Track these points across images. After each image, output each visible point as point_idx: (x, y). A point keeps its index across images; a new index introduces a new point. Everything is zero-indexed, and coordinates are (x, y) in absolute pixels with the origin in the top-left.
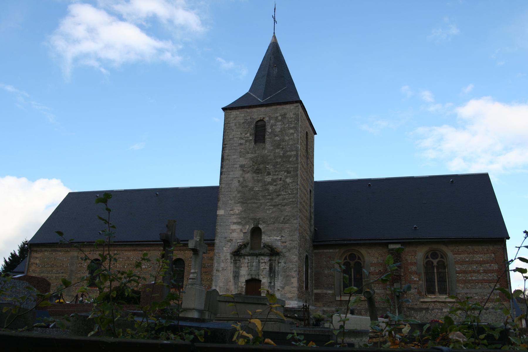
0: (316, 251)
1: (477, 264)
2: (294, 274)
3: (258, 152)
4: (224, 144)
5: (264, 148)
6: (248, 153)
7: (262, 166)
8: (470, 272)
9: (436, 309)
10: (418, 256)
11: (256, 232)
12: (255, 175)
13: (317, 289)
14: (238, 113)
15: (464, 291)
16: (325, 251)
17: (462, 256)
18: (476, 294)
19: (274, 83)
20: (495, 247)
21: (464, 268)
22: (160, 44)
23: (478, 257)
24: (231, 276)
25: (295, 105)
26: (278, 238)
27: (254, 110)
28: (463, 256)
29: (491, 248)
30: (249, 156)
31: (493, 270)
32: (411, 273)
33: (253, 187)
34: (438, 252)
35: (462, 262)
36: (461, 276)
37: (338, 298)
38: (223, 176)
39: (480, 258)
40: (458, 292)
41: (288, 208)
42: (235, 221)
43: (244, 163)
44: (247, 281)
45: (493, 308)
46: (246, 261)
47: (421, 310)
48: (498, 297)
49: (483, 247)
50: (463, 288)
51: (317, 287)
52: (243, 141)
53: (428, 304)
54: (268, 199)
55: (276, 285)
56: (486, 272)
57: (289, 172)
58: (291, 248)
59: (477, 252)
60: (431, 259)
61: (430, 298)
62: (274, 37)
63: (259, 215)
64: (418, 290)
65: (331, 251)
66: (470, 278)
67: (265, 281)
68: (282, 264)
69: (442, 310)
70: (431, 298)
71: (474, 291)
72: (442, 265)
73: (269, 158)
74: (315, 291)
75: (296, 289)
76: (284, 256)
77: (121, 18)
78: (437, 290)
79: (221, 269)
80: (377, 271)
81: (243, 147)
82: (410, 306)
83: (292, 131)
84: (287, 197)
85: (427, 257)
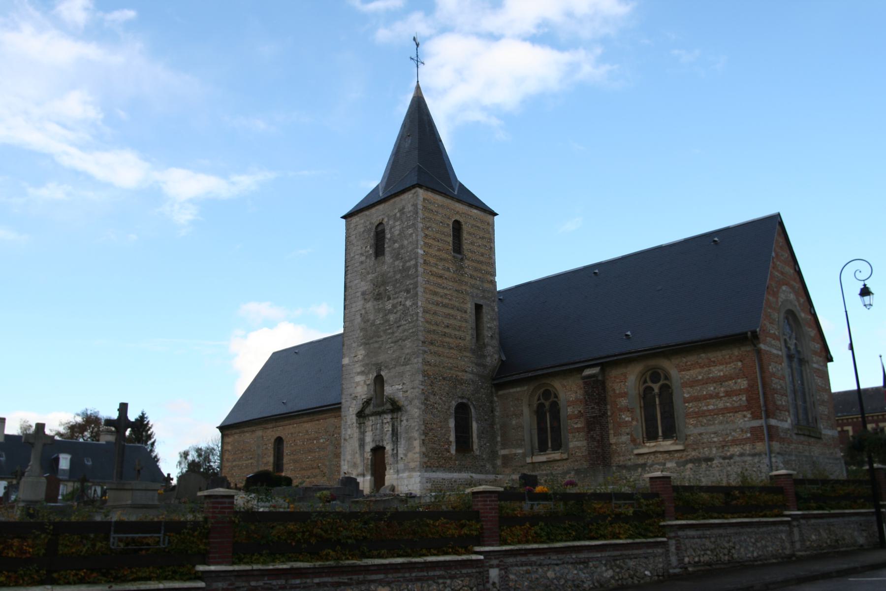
0: (500, 393)
1: (715, 382)
2: (416, 434)
3: (378, 269)
4: (346, 267)
5: (384, 263)
6: (368, 273)
7: (382, 289)
8: (705, 398)
9: (657, 464)
10: (627, 383)
11: (379, 381)
12: (375, 303)
13: (504, 449)
14: (358, 219)
15: (696, 431)
16: (512, 390)
17: (691, 372)
18: (715, 433)
19: (420, 154)
20: (743, 349)
21: (695, 391)
22: (565, 57)
23: (717, 371)
24: (357, 445)
25: (413, 191)
26: (400, 387)
27: (373, 210)
28: (693, 373)
29: (736, 352)
30: (370, 277)
31: (740, 390)
32: (620, 410)
33: (374, 320)
34: (660, 371)
35: (693, 383)
36: (691, 407)
37: (529, 460)
38: (347, 311)
39: (720, 371)
40: (689, 433)
41: (408, 343)
42: (359, 370)
43: (365, 288)
44: (372, 450)
45: (741, 455)
46: (370, 423)
47: (636, 467)
48: (749, 435)
49: (724, 352)
50: (695, 426)
51: (504, 446)
52: (363, 258)
53: (646, 457)
54: (389, 334)
55: (399, 452)
56: (728, 394)
57: (408, 291)
58: (413, 399)
59: (714, 362)
60: (661, 382)
61: (650, 447)
62: (418, 88)
63: (382, 358)
64: (632, 436)
65: (518, 389)
66: (705, 408)
67: (388, 448)
68: (404, 423)
69: (664, 464)
70: (649, 447)
71: (711, 429)
72: (666, 389)
73: (389, 275)
74: (503, 452)
75: (417, 455)
76: (406, 411)
77: (494, 37)
78: (660, 433)
79: (347, 437)
80: (576, 412)
81: (363, 266)
82: (621, 463)
83: (410, 231)
84: (406, 327)
85: (645, 382)
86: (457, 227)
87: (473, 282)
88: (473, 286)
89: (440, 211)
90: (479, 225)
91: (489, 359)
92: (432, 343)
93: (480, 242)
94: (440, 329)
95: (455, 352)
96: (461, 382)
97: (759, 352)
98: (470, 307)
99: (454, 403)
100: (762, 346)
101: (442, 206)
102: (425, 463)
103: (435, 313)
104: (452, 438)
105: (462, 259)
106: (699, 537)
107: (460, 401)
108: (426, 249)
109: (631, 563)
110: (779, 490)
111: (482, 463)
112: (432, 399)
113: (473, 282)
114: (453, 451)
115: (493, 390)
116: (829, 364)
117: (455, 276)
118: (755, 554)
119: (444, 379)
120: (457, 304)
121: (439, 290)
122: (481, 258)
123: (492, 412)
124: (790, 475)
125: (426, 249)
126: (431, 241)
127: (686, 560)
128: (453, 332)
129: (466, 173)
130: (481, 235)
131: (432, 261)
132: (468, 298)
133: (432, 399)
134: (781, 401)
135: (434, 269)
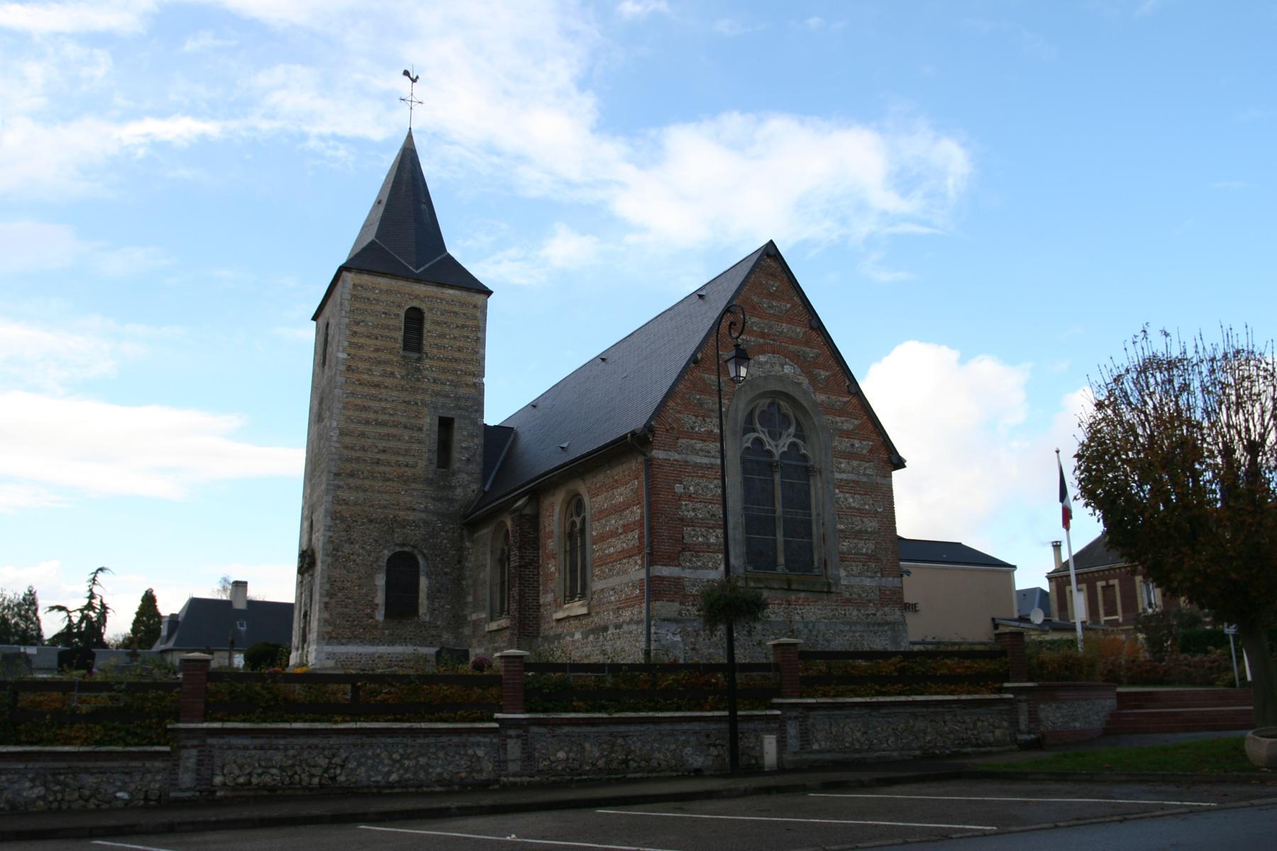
49: (625, 466)
74: (474, 617)
86: (415, 319)
87: (438, 388)
88: (436, 394)
89: (384, 297)
90: (456, 309)
91: (459, 491)
92: (352, 475)
93: (456, 333)
94: (369, 455)
95: (395, 484)
96: (404, 524)
97: (649, 463)
98: (429, 422)
99: (387, 553)
100: (658, 454)
101: (388, 292)
102: (327, 633)
103: (363, 435)
104: (380, 598)
105: (419, 360)
106: (262, 748)
107: (398, 549)
108: (352, 351)
109: (90, 780)
110: (495, 680)
111: (434, 633)
112: (347, 548)
113: (438, 388)
114: (380, 616)
115: (465, 532)
116: (896, 474)
117: (403, 382)
118: (394, 777)
119: (371, 521)
120: (404, 420)
121: (371, 404)
122: (457, 355)
123: (459, 562)
124: (521, 657)
125: (352, 351)
126: (362, 341)
127: (218, 780)
128: (393, 458)
129: (461, 244)
130: (460, 322)
131: (362, 366)
132: (426, 410)
133: (347, 548)
134: (694, 536)
135: (366, 376)
